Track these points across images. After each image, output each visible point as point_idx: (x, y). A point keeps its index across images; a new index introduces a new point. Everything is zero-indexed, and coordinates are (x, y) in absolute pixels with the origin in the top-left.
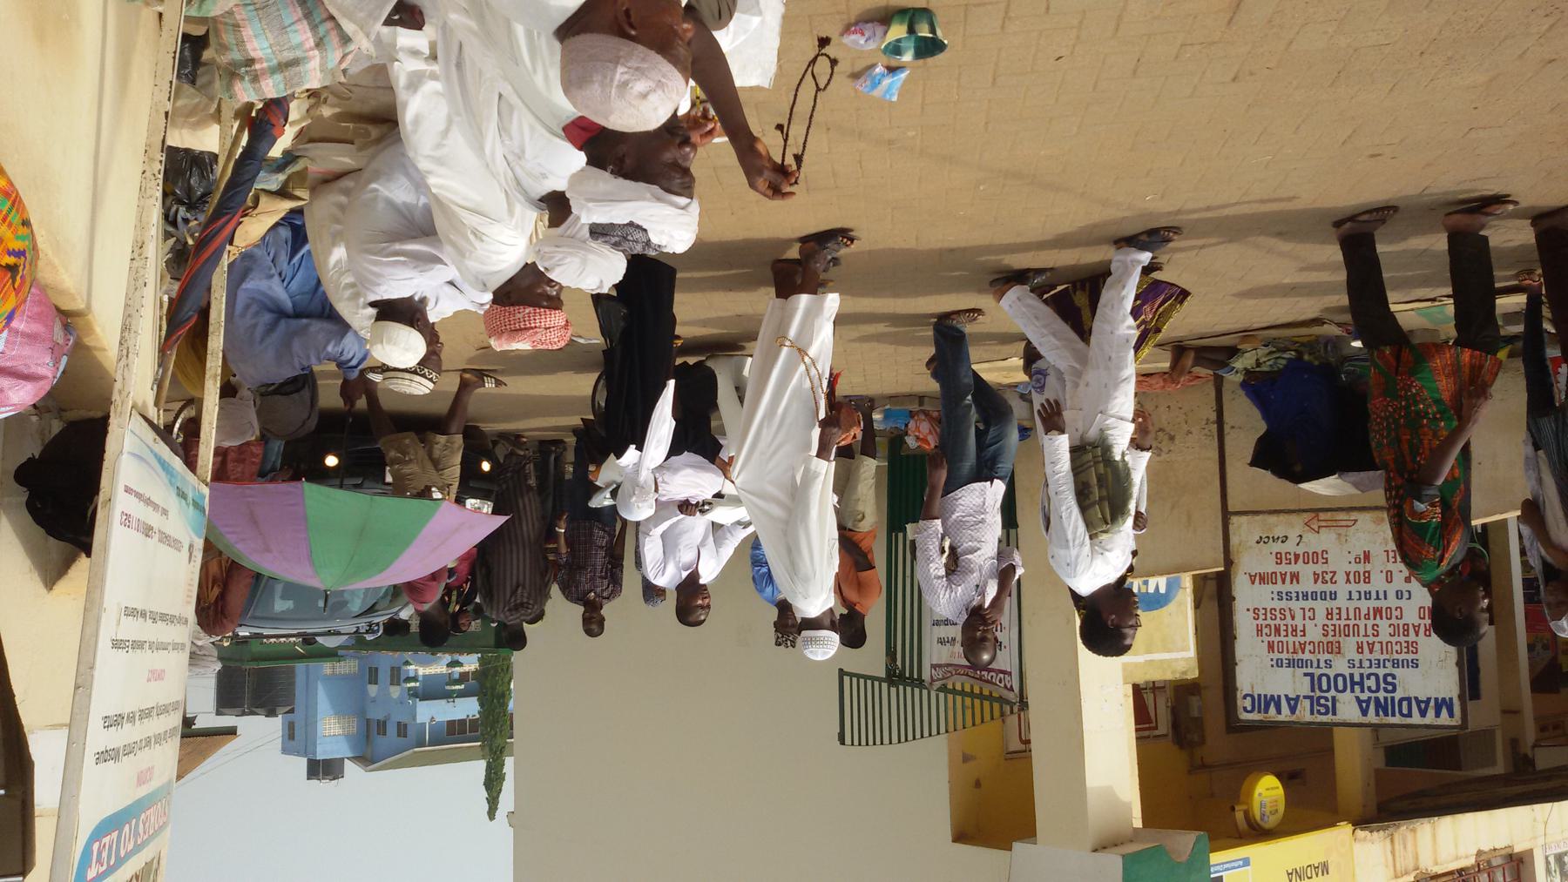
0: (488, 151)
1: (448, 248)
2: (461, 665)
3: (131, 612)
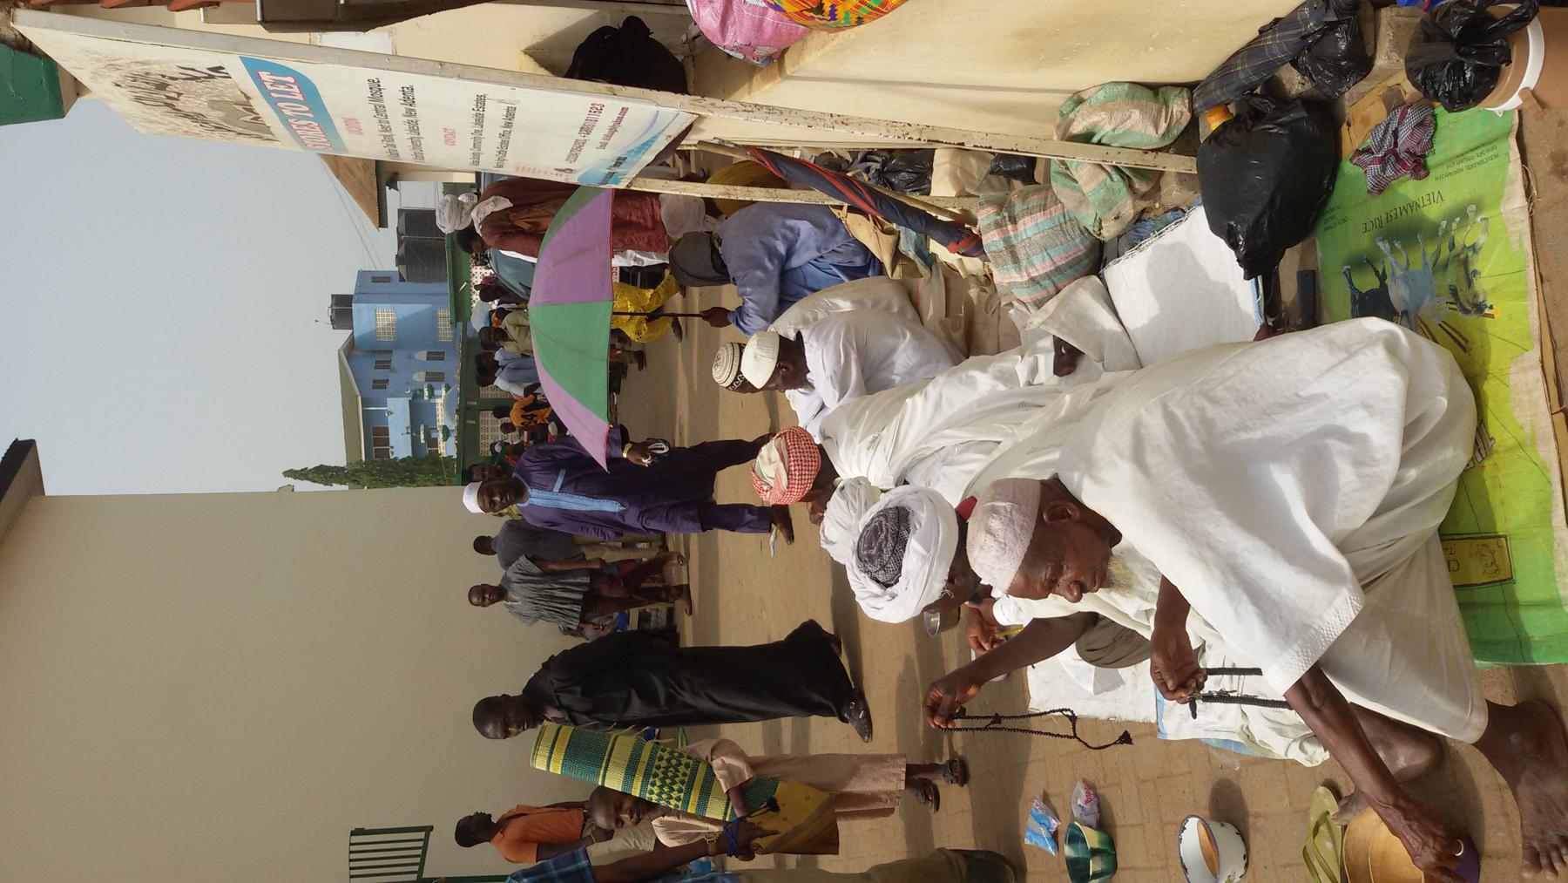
0: (947, 432)
1: (853, 400)
2: (446, 438)
3: (510, 113)
